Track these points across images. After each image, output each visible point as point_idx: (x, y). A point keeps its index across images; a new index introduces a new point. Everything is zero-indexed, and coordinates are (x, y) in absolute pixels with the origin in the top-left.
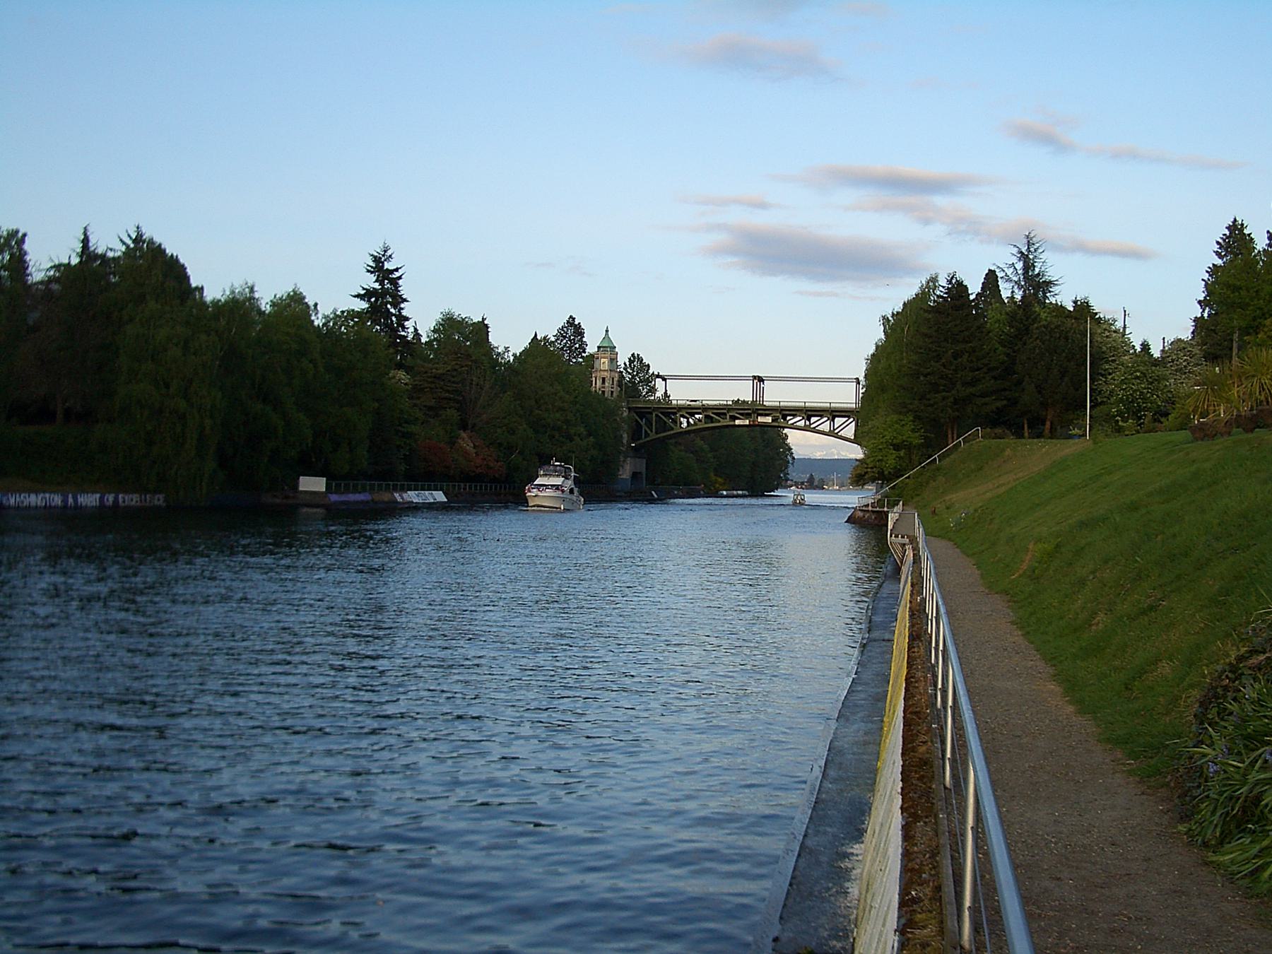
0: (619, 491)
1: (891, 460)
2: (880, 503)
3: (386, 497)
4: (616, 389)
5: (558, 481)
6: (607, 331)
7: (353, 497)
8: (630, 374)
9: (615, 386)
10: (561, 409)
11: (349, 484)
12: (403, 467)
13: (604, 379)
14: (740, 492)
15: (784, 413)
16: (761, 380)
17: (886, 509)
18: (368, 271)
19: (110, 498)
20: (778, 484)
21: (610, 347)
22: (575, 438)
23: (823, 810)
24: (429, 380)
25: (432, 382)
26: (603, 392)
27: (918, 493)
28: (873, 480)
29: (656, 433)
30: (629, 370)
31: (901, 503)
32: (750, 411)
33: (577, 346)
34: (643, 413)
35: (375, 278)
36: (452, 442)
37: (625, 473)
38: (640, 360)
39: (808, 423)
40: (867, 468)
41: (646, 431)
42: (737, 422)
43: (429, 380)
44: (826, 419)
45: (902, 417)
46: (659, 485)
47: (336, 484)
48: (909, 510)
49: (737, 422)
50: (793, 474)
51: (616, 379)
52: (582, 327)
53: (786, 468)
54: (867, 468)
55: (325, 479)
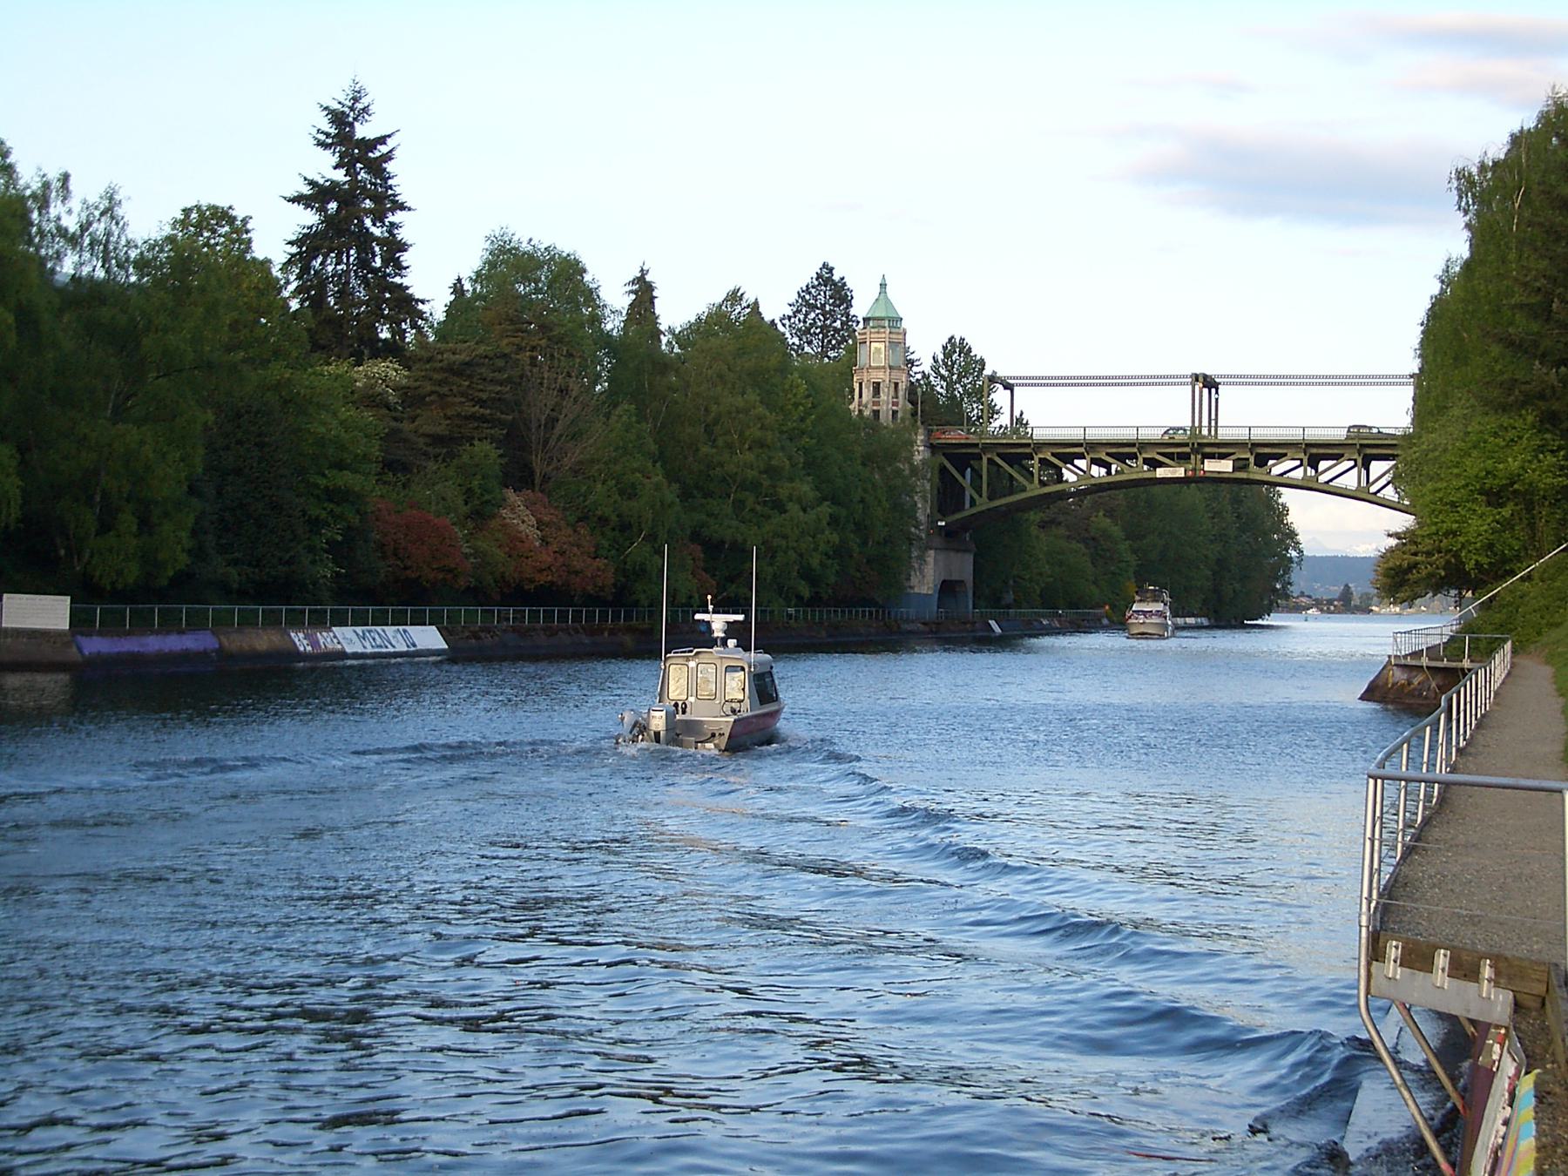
0: (908, 621)
1: (1479, 524)
2: (1453, 646)
3: (263, 640)
4: (903, 405)
5: (1160, 607)
6: (883, 286)
7: (154, 644)
8: (943, 377)
9: (901, 399)
10: (761, 444)
11: (154, 608)
12: (326, 571)
13: (877, 388)
14: (1190, 621)
15: (1266, 452)
16: (1210, 383)
17: (1466, 664)
18: (321, 144)
19: (1199, 620)
20: (1271, 603)
21: (890, 319)
22: (790, 506)
23: (1404, 1144)
24: (436, 376)
25: (440, 383)
26: (876, 413)
27: (1557, 618)
28: (1438, 585)
29: (990, 498)
30: (943, 372)
31: (1508, 646)
32: (1187, 450)
33: (838, 324)
34: (963, 457)
35: (335, 159)
36: (481, 514)
37: (926, 578)
38: (965, 350)
39: (1311, 472)
40: (1415, 554)
41: (971, 497)
42: (1161, 473)
43: (436, 376)
44: (1352, 463)
45: (1505, 421)
46: (1009, 607)
47: (352, 610)
48: (1528, 664)
49: (1161, 473)
50: (1299, 581)
51: (902, 386)
52: (849, 285)
53: (1286, 572)
54: (1415, 554)
55: (68, 598)
